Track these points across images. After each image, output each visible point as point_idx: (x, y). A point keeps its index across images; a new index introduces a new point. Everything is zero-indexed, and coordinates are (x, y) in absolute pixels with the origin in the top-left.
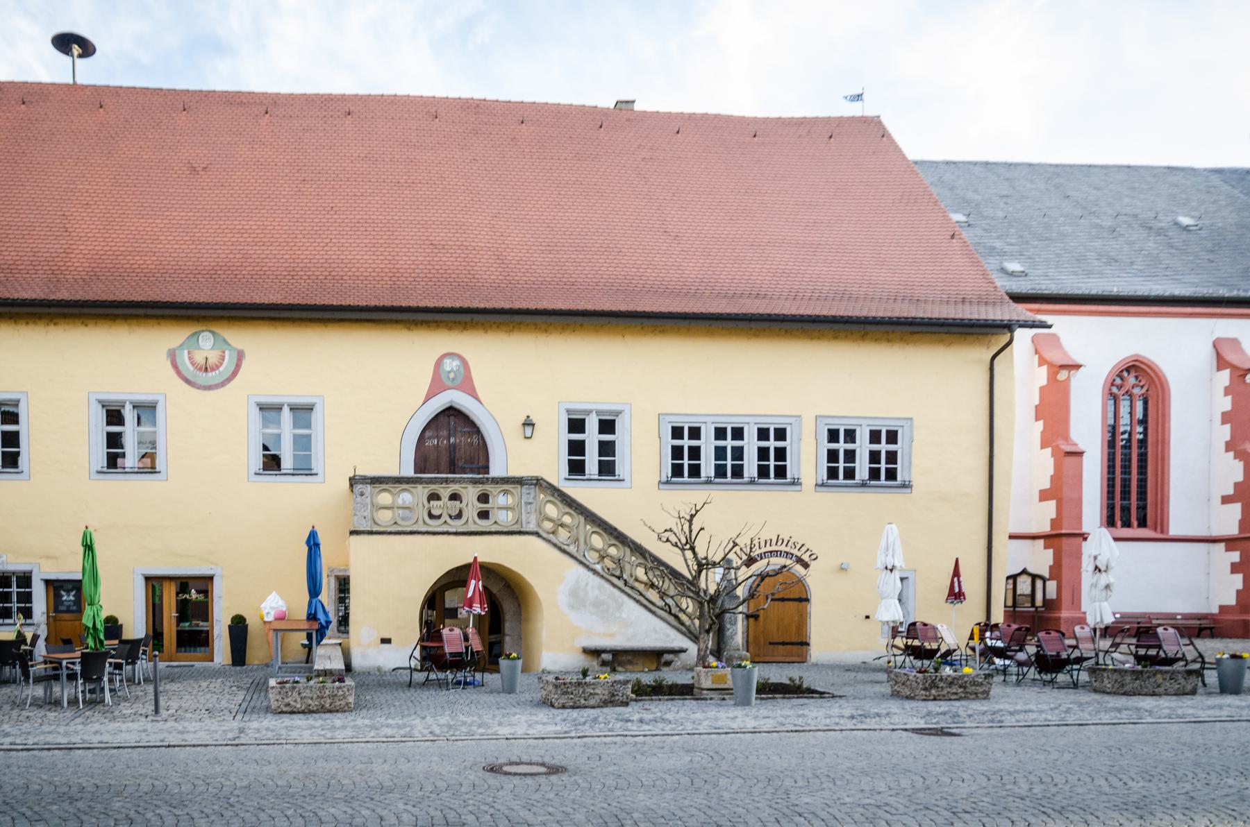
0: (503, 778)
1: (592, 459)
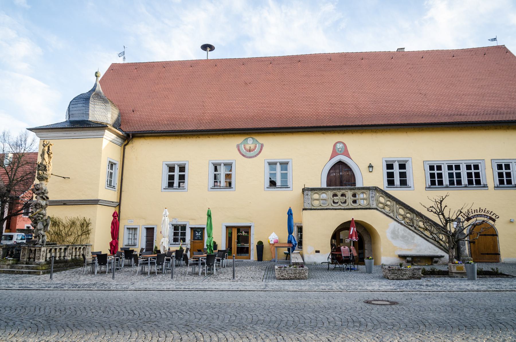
0: (373, 306)
1: (397, 179)
